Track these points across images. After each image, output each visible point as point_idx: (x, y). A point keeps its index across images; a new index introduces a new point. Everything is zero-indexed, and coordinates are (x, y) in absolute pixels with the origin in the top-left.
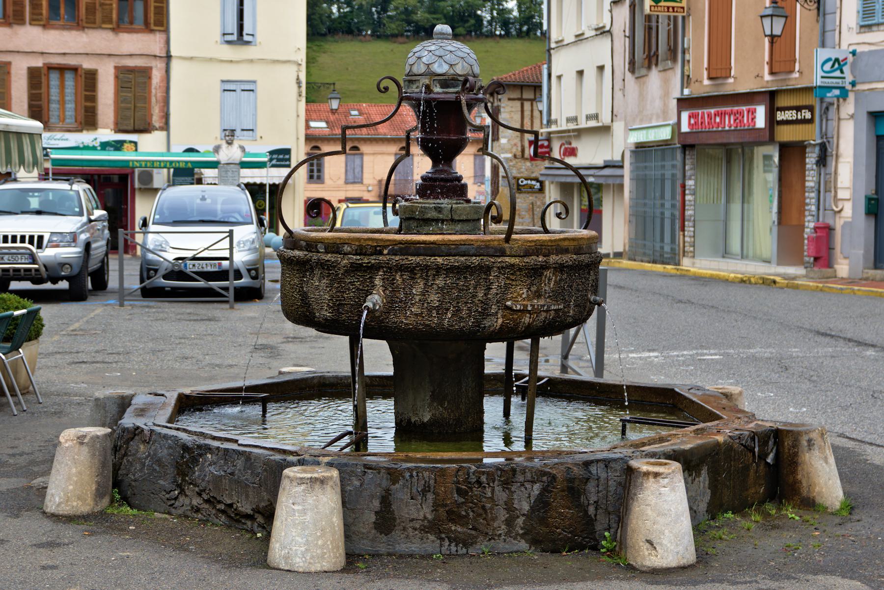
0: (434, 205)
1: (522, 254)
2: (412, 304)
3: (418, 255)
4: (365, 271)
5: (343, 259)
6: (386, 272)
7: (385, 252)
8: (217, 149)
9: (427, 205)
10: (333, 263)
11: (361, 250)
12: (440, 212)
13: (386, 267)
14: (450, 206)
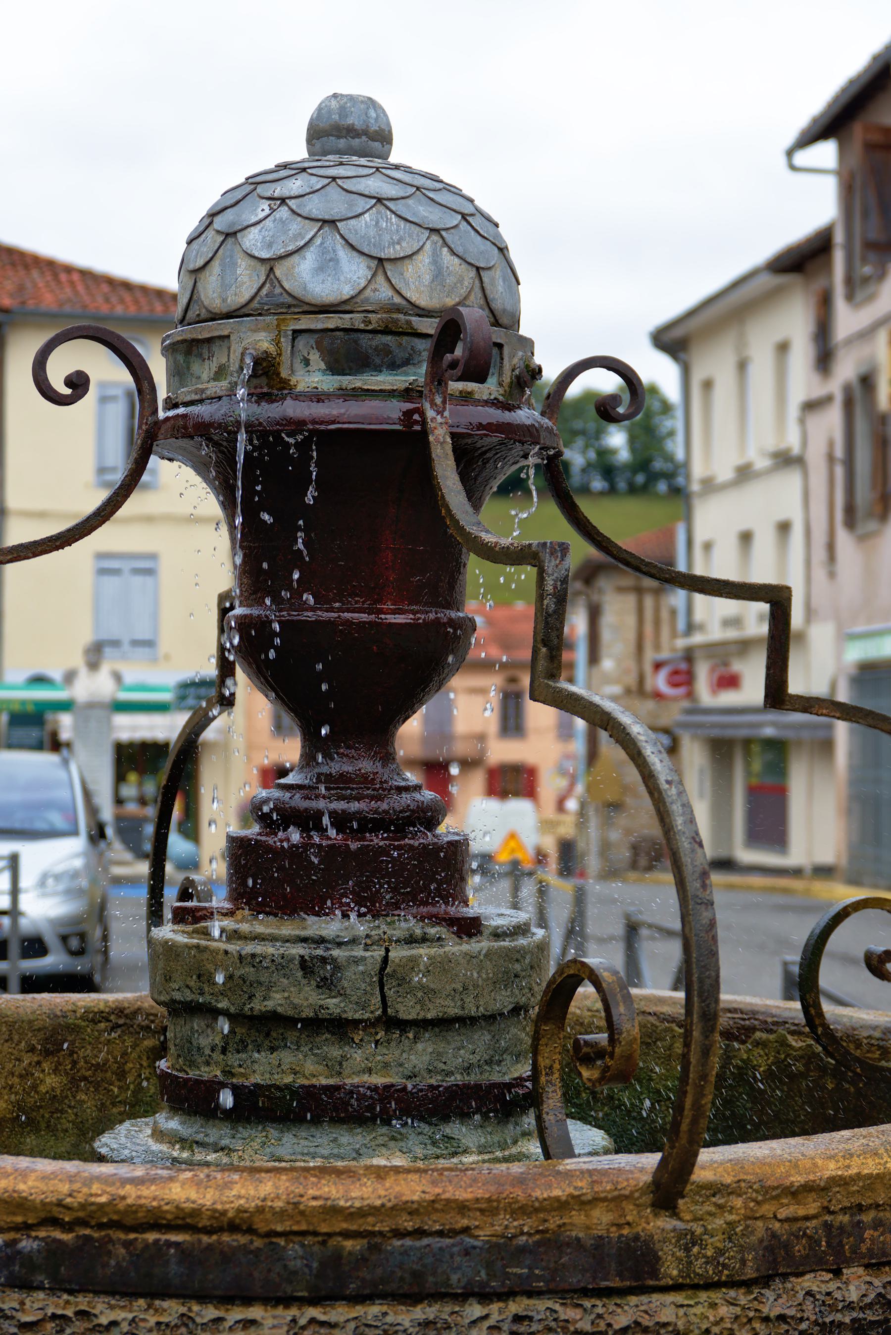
0: (298, 950)
1: (750, 1273)
8: (70, 677)
9: (269, 949)
12: (326, 984)
14: (378, 953)
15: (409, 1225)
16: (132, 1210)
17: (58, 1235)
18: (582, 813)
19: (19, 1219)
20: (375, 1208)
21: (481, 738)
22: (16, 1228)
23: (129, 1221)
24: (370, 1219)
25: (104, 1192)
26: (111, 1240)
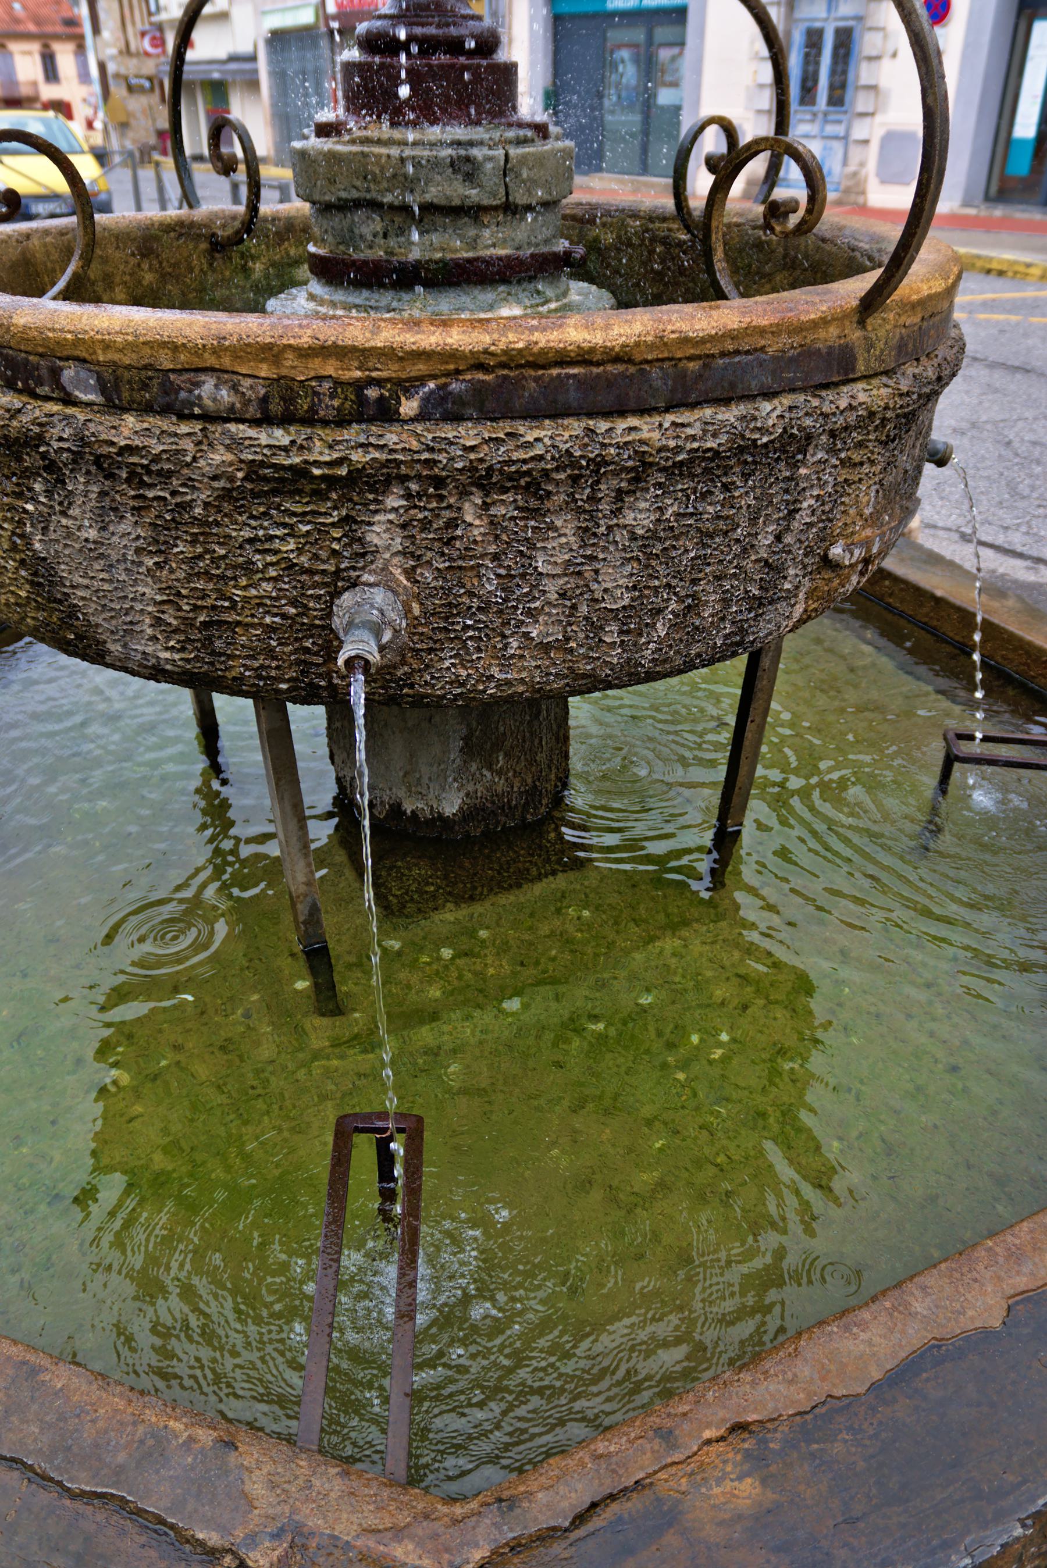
0: (447, 152)
2: (529, 613)
3: (556, 414)
4: (319, 495)
5: (205, 442)
6: (419, 496)
7: (409, 407)
10: (157, 459)
11: (289, 399)
13: (419, 477)
14: (500, 153)
15: (731, 348)
16: (543, 352)
17: (481, 376)
18: (106, 130)
19: (452, 367)
20: (712, 336)
21: (35, 84)
22: (447, 374)
23: (541, 361)
24: (708, 345)
25: (520, 340)
26: (524, 377)
